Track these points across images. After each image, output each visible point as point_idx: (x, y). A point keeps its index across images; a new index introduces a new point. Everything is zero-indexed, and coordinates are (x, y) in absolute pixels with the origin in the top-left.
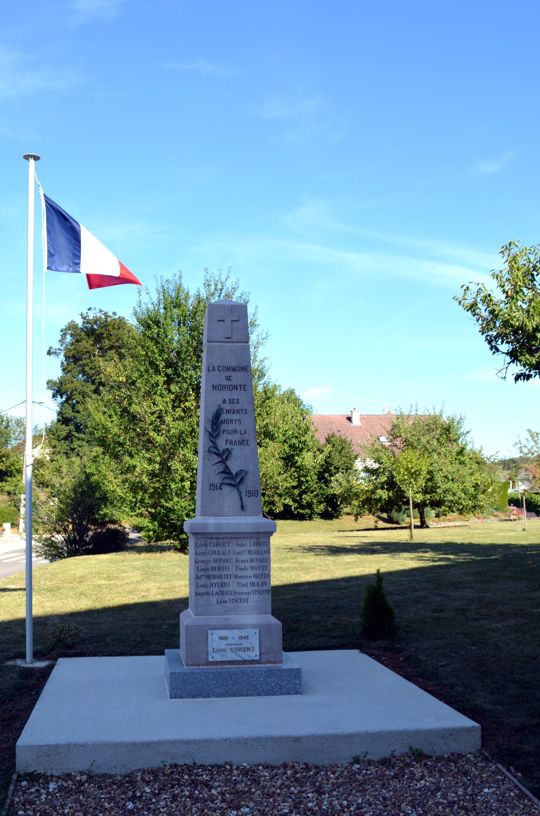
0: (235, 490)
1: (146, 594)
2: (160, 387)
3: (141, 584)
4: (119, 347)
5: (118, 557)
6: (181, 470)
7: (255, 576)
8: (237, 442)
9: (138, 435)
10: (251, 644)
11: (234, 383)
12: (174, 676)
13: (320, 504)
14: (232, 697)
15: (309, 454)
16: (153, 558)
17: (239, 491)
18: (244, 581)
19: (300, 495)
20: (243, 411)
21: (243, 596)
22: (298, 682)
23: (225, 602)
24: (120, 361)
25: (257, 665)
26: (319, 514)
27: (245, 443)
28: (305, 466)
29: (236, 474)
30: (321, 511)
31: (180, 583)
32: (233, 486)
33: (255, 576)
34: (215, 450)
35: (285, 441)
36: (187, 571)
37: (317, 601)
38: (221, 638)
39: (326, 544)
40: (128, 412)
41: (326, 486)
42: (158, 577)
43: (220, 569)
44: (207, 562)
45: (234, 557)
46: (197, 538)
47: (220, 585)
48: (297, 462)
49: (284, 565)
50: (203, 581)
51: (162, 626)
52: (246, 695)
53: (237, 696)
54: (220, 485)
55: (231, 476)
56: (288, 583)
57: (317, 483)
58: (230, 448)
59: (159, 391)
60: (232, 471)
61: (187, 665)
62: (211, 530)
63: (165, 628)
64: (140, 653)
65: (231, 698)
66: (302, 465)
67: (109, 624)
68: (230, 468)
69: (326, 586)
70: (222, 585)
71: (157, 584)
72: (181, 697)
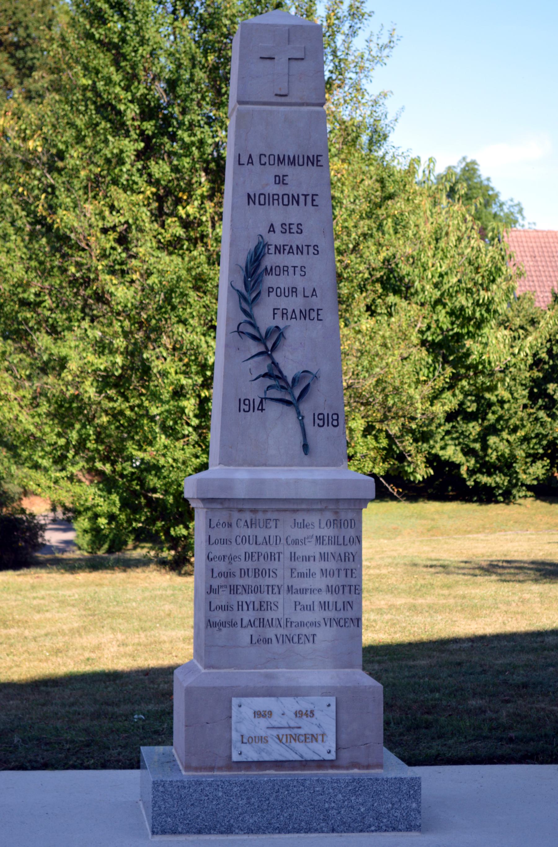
0: (290, 412)
1: (93, 655)
2: (128, 166)
3: (80, 635)
4: (17, 46)
5: (21, 579)
6: (176, 373)
7: (330, 589)
8: (297, 313)
9: (73, 282)
10: (319, 726)
11: (292, 189)
12: (161, 789)
13: (534, 462)
14: (279, 833)
15: (499, 335)
16: (106, 582)
17: (299, 413)
18: (307, 599)
19: (483, 438)
20: (311, 249)
21: (305, 631)
22: (414, 805)
23: (268, 641)
24: (21, 83)
25: (331, 771)
26: (530, 488)
27: (314, 315)
28: (490, 363)
29: (294, 380)
30: (537, 479)
31: (174, 633)
32: (288, 403)
33: (330, 589)
34: (250, 330)
35: (439, 302)
36: (189, 609)
37: (484, 672)
38: (258, 714)
39: (532, 557)
40: (49, 228)
41: (548, 416)
42: (120, 621)
43: (257, 573)
44: (232, 558)
45: (287, 550)
46: (212, 509)
47: (257, 606)
48: (468, 354)
49: (420, 601)
50: (223, 598)
51: (133, 715)
52: (308, 830)
53: (289, 832)
54: (261, 402)
55: (283, 384)
56: (425, 637)
57: (525, 406)
58: (281, 327)
59: (125, 176)
60: (285, 373)
61: (188, 768)
62: (240, 493)
63: (140, 719)
64: (86, 764)
65: (277, 836)
66: (482, 363)
67: (13, 711)
68: (281, 366)
69: (512, 643)
70: (262, 606)
71: (119, 636)
72: (174, 832)
